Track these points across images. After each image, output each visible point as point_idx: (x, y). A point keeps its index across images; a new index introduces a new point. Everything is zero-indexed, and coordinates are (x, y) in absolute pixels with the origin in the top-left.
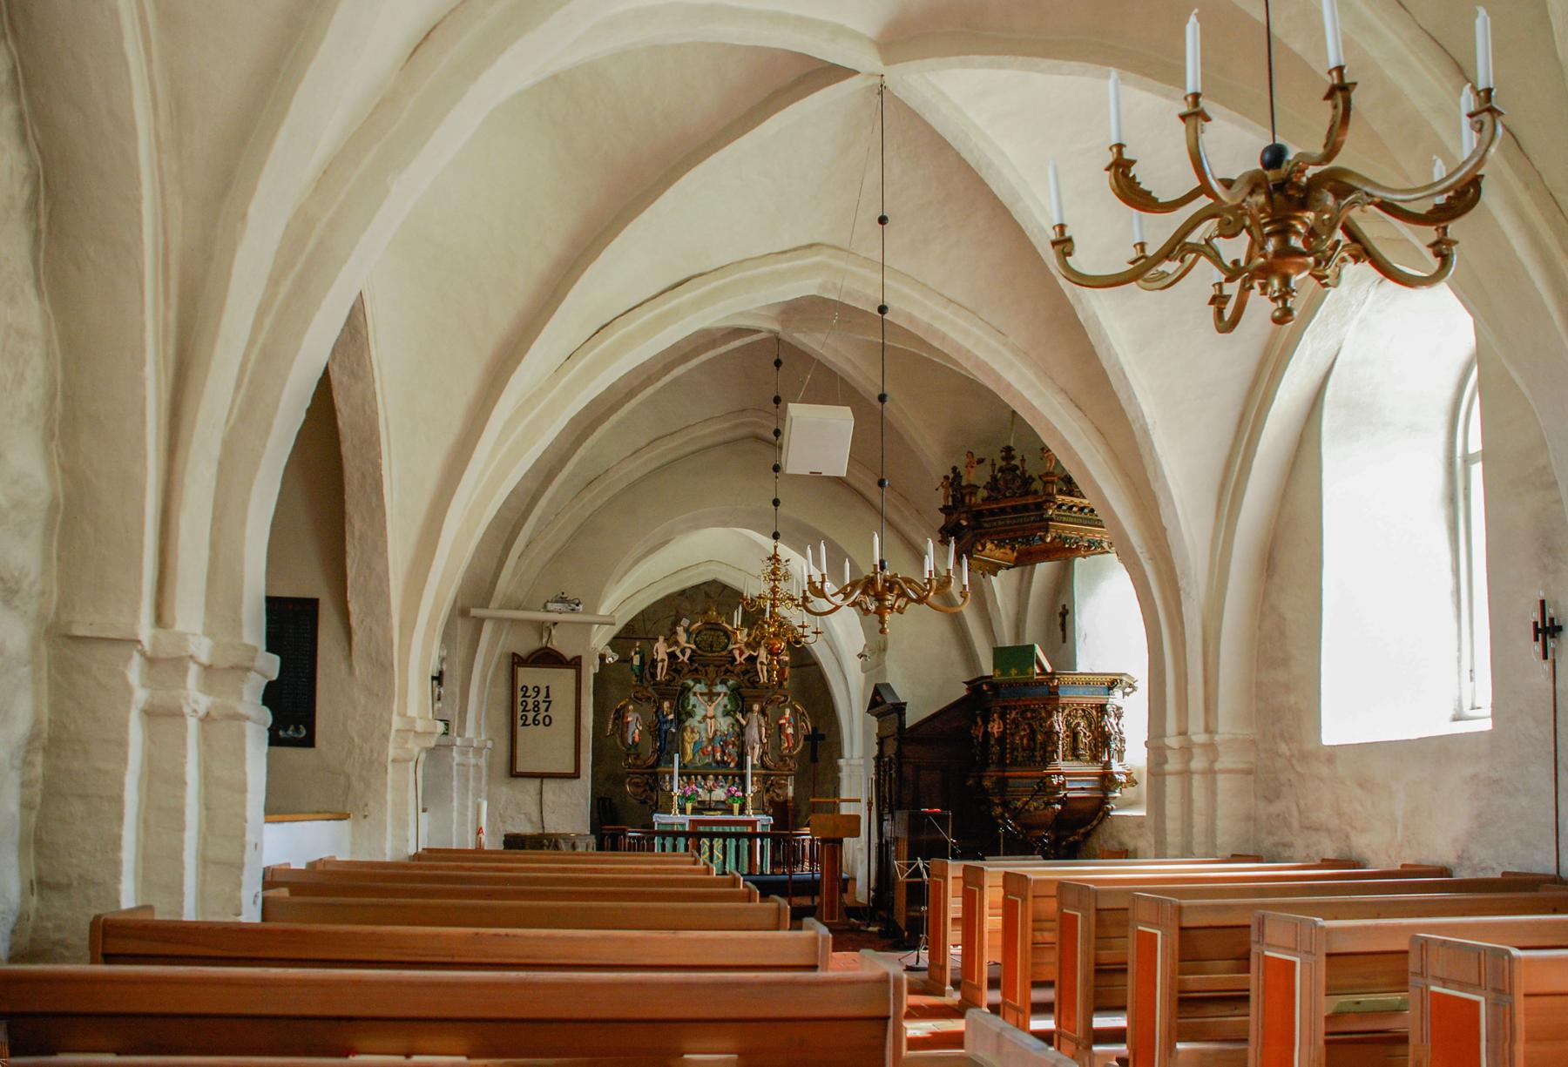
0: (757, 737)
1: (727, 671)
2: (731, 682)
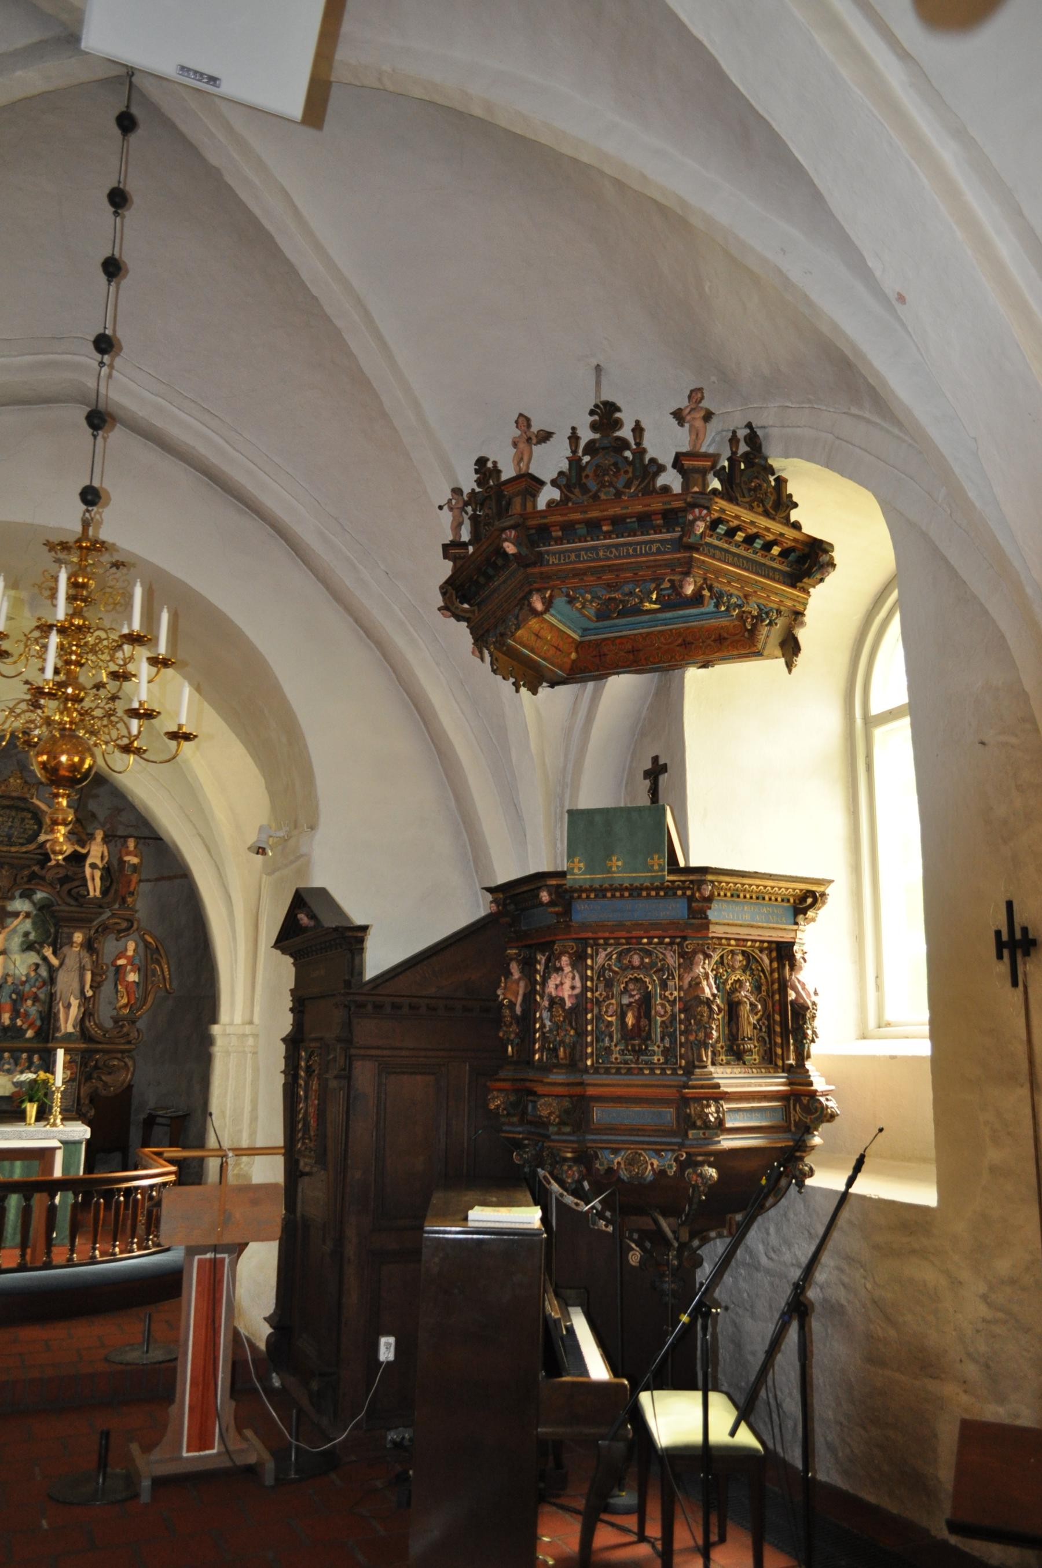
0: (76, 986)
1: (33, 876)
2: (39, 895)
